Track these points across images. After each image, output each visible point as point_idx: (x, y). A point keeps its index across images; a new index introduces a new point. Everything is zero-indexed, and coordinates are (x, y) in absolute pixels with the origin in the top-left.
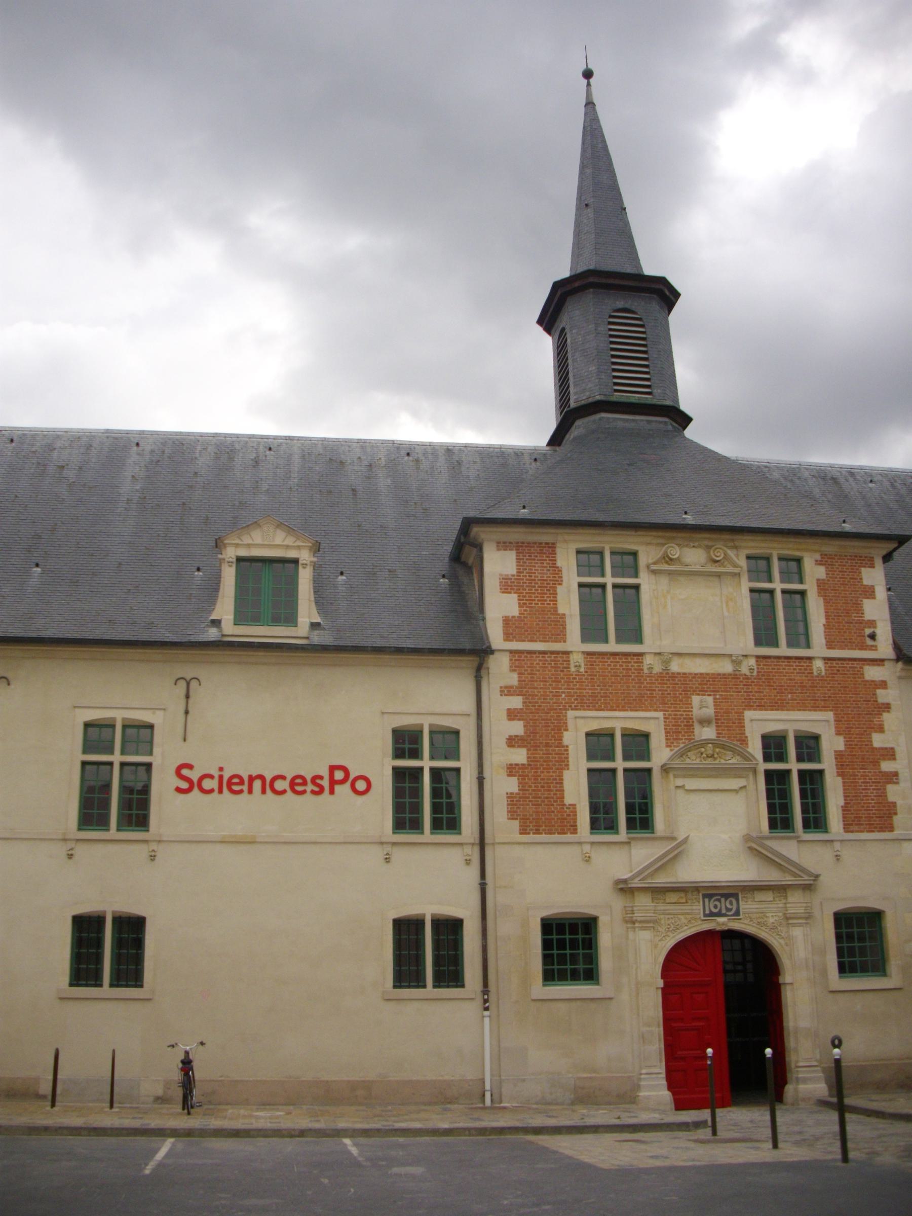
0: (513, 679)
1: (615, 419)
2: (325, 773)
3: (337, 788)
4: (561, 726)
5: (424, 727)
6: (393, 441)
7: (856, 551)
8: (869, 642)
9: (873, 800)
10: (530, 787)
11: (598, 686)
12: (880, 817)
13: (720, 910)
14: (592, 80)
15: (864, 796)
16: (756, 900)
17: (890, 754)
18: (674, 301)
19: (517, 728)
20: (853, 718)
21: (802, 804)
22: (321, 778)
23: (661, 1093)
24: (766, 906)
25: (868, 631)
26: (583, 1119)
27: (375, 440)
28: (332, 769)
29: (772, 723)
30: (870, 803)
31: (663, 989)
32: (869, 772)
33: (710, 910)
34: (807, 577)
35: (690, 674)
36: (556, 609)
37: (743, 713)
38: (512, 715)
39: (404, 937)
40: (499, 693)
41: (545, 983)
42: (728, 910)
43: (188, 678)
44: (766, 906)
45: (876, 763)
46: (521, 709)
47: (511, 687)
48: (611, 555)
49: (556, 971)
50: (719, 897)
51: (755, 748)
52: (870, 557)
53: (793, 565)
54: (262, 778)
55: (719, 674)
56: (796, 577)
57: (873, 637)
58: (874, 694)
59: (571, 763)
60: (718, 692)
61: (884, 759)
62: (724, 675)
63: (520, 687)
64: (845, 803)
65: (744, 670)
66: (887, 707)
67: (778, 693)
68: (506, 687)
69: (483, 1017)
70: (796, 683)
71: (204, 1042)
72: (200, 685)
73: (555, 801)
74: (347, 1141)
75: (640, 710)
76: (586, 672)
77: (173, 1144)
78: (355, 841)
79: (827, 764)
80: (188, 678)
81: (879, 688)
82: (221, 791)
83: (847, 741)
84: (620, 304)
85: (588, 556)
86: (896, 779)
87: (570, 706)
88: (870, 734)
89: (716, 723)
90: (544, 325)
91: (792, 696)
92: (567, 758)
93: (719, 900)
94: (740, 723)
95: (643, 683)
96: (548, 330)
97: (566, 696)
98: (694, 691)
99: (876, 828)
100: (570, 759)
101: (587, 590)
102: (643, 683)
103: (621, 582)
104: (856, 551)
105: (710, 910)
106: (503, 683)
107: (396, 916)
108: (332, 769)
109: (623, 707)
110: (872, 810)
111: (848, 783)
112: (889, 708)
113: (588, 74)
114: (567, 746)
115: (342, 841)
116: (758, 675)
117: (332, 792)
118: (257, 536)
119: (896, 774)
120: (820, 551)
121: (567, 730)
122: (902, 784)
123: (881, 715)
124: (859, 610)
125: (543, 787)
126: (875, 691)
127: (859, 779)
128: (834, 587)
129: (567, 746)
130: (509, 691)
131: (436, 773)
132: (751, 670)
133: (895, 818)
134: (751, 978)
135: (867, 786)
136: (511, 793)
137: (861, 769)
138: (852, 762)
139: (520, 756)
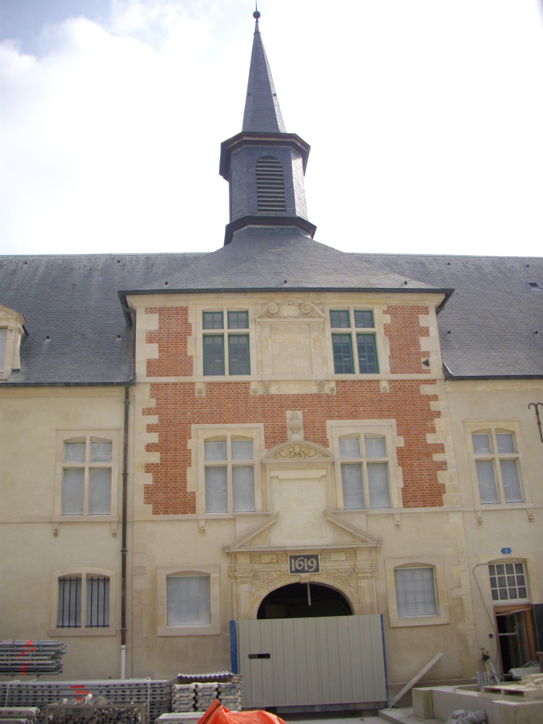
4: (186, 436)
8: (424, 367)
9: (427, 482)
12: (431, 495)
16: (332, 559)
17: (440, 448)
18: (306, 151)
25: (423, 360)
32: (423, 462)
33: (296, 568)
36: (186, 353)
40: (142, 414)
45: (429, 455)
46: (157, 424)
47: (151, 409)
57: (427, 363)
58: (428, 405)
61: (435, 452)
62: (311, 395)
64: (404, 486)
80: (536, 404)
83: (406, 440)
85: (213, 339)
86: (445, 467)
87: (194, 421)
89: (305, 430)
92: (190, 458)
93: (303, 561)
97: (191, 414)
98: (287, 407)
100: (192, 459)
105: (296, 568)
112: (440, 415)
113: (257, 15)
116: (337, 394)
119: (445, 463)
123: (433, 420)
124: (417, 345)
125: (171, 480)
126: (429, 403)
129: (190, 450)
130: (149, 412)
133: (444, 496)
137: (417, 460)
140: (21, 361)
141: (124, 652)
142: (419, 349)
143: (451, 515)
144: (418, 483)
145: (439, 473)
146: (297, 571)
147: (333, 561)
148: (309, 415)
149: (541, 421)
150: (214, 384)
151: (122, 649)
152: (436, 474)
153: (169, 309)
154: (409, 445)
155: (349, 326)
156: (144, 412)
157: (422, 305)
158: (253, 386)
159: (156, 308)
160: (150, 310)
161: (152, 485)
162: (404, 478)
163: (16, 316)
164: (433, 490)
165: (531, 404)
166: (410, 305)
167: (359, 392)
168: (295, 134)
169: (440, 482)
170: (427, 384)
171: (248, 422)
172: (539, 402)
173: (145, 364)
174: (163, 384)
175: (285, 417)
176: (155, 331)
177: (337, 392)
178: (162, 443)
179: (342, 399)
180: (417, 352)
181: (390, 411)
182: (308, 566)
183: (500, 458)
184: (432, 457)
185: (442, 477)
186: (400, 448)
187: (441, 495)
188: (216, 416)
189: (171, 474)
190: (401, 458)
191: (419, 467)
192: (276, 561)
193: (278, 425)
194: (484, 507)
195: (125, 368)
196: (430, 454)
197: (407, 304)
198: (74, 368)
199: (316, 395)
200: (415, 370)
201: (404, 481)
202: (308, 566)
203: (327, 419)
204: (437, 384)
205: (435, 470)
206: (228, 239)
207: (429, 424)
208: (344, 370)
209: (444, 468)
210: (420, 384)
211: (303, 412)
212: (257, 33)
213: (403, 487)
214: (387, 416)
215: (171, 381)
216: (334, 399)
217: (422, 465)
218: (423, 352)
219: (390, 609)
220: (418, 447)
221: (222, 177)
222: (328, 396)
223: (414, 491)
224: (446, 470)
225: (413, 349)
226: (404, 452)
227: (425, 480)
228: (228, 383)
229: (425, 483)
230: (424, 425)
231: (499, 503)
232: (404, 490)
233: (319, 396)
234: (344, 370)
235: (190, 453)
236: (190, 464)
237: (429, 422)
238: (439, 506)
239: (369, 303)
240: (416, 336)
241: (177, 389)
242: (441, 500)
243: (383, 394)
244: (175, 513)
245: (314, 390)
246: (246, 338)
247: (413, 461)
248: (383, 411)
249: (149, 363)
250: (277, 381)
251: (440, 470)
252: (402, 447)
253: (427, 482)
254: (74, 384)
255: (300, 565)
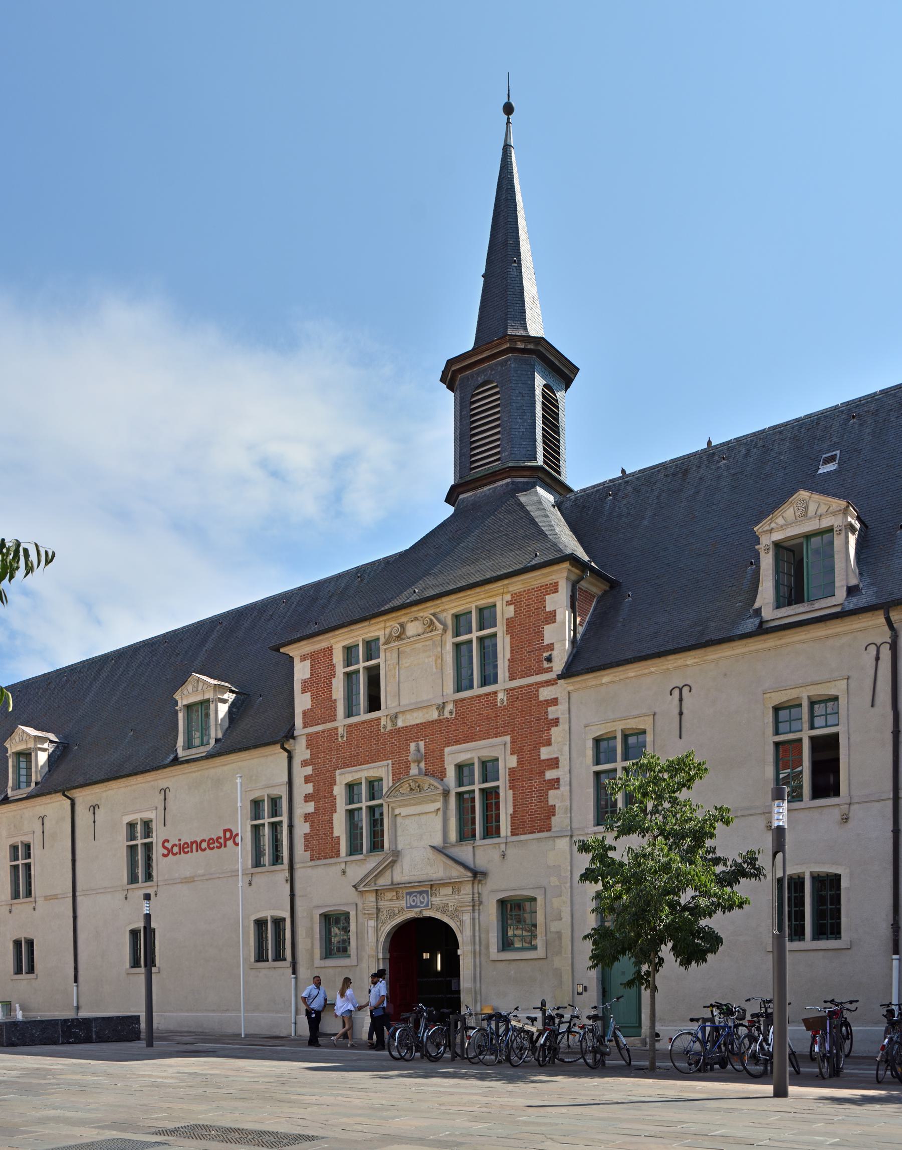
0: (307, 755)
1: (313, 1051)
2: (222, 835)
3: (228, 843)
4: (333, 783)
5: (806, 874)
6: (827, 940)
7: (539, 582)
8: (546, 665)
9: (536, 805)
10: (316, 828)
11: (354, 748)
12: (540, 820)
13: (416, 904)
14: (849, 680)
15: (529, 803)
16: (386, 899)
17: (554, 763)
18: (572, 376)
19: (309, 788)
20: (526, 737)
21: (803, 919)
22: (221, 838)
23: (669, 1064)
24: (447, 898)
25: (546, 654)
26: (154, 789)
27: (744, 436)
28: (225, 831)
29: (529, 907)
30: (533, 809)
31: (390, 959)
32: (534, 782)
33: (411, 904)
34: (772, 760)
35: (410, 726)
36: (331, 697)
37: (444, 750)
38: (307, 779)
39: (494, 824)
40: (300, 766)
41: (261, 817)
42: (422, 903)
43: (879, 642)
44: (447, 898)
45: (542, 773)
46: (312, 775)
47: (307, 760)
48: (600, 764)
49: (619, 757)
50: (416, 894)
51: (451, 773)
52: (555, 583)
53: (819, 709)
54: (196, 842)
55: (429, 722)
56: (611, 742)
57: (549, 659)
58: (545, 713)
59: (338, 808)
60: (428, 736)
61: (549, 769)
62: (432, 721)
63: (311, 759)
64: (514, 812)
65: (447, 714)
66: (556, 722)
67: (469, 728)
68: (304, 761)
69: (892, 960)
70: (483, 717)
71: (588, 989)
72: (690, 691)
73: (329, 836)
74: (781, 776)
75: (377, 762)
76: (347, 740)
77: (854, 1026)
78: (356, 953)
79: (502, 783)
80: (681, 687)
81: (551, 706)
82: (180, 854)
83: (519, 759)
84: (536, 298)
85: (781, 722)
86: (558, 785)
87: (338, 767)
88: (539, 749)
89: (425, 761)
90: (447, 383)
91: (480, 728)
92: (336, 804)
93: (416, 896)
94: (441, 758)
95: (380, 740)
96: (451, 387)
97: (336, 760)
98: (412, 739)
99: (536, 829)
100: (337, 805)
101: (602, 756)
102: (380, 740)
103: (809, 884)
104: (539, 582)
105: (411, 904)
106: (559, 707)
107: (497, 685)
108: (225, 831)
109: (368, 761)
110: (535, 814)
111: (517, 794)
112: (558, 722)
113: (508, 109)
114: (336, 796)
115: (846, 695)
116: (456, 716)
117: (225, 846)
118: (788, 512)
119: (557, 780)
120: (509, 592)
121: (335, 785)
122: (562, 789)
123: (550, 730)
124: (540, 634)
125: (322, 827)
126: (547, 709)
127: (526, 789)
128: (531, 655)
129: (336, 796)
130: (305, 763)
131: (371, 809)
132: (451, 713)
133: (553, 819)
134: (771, 1050)
135: (532, 794)
136: (306, 834)
137: (529, 780)
138: (522, 776)
139: (310, 807)
140: (897, 636)
141: (895, 963)
142: (542, 643)
143: (558, 841)
144: (528, 807)
145: (551, 793)
146: (412, 907)
147: (444, 885)
148: (430, 744)
149: (685, 711)
150: (352, 725)
151: (892, 960)
152: (547, 795)
153: (318, 652)
154: (521, 764)
155: (800, 740)
156: (302, 764)
157: (551, 582)
158: (383, 722)
159: (308, 654)
160: (303, 658)
161: (309, 833)
162: (513, 803)
163: (480, 885)
164: (542, 813)
165: (674, 688)
166: (537, 586)
167: (477, 709)
168: (29, 556)
169: (551, 803)
170: (548, 686)
171: (379, 761)
172: (686, 683)
173: (620, 732)
174: (315, 734)
175: (409, 750)
176: (308, 679)
177: (456, 714)
178: (315, 793)
179: (460, 721)
180: (539, 647)
181: (505, 726)
182: (420, 901)
183: (773, 735)
184: (544, 775)
185: (554, 797)
186: (513, 768)
187: (550, 818)
188: (354, 759)
189: (322, 822)
190: (513, 780)
191: (530, 789)
192: (395, 898)
193: (403, 760)
194: (380, 836)
195: (639, 740)
196: (543, 772)
197: (532, 585)
198: (284, 621)
199: (436, 720)
200: (535, 671)
201: (514, 806)
202: (420, 901)
203: (445, 747)
204: (342, 999)
205: (546, 789)
206: (452, 390)
207: (545, 736)
208: (457, 996)
209: (556, 786)
210: (539, 687)
211: (425, 742)
212: (507, 148)
213: (512, 813)
214: (503, 733)
215: (490, 691)
216: (452, 723)
217: (534, 785)
218: (546, 645)
219: (490, 942)
220: (530, 766)
221: (30, 553)
222: (447, 720)
223: (523, 816)
224: (558, 788)
225: (535, 645)
226: (516, 773)
227: (535, 803)
228: (478, 696)
229: (535, 806)
230: (540, 737)
231: (281, 822)
232: (513, 816)
233: (439, 721)
234: (457, 996)
235: (335, 799)
236: (335, 809)
237: (544, 733)
238: (547, 831)
239: (490, 597)
240: (540, 626)
241: (325, 737)
242: (550, 824)
243: (500, 707)
244: (326, 858)
245: (434, 715)
246: (601, 743)
247: (524, 783)
248: (499, 727)
249: (305, 713)
250: (403, 712)
251: (552, 789)
252: (514, 768)
253: (536, 805)
254: (351, 790)
255: (414, 901)
